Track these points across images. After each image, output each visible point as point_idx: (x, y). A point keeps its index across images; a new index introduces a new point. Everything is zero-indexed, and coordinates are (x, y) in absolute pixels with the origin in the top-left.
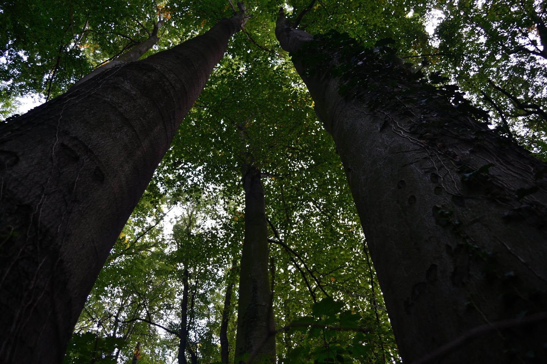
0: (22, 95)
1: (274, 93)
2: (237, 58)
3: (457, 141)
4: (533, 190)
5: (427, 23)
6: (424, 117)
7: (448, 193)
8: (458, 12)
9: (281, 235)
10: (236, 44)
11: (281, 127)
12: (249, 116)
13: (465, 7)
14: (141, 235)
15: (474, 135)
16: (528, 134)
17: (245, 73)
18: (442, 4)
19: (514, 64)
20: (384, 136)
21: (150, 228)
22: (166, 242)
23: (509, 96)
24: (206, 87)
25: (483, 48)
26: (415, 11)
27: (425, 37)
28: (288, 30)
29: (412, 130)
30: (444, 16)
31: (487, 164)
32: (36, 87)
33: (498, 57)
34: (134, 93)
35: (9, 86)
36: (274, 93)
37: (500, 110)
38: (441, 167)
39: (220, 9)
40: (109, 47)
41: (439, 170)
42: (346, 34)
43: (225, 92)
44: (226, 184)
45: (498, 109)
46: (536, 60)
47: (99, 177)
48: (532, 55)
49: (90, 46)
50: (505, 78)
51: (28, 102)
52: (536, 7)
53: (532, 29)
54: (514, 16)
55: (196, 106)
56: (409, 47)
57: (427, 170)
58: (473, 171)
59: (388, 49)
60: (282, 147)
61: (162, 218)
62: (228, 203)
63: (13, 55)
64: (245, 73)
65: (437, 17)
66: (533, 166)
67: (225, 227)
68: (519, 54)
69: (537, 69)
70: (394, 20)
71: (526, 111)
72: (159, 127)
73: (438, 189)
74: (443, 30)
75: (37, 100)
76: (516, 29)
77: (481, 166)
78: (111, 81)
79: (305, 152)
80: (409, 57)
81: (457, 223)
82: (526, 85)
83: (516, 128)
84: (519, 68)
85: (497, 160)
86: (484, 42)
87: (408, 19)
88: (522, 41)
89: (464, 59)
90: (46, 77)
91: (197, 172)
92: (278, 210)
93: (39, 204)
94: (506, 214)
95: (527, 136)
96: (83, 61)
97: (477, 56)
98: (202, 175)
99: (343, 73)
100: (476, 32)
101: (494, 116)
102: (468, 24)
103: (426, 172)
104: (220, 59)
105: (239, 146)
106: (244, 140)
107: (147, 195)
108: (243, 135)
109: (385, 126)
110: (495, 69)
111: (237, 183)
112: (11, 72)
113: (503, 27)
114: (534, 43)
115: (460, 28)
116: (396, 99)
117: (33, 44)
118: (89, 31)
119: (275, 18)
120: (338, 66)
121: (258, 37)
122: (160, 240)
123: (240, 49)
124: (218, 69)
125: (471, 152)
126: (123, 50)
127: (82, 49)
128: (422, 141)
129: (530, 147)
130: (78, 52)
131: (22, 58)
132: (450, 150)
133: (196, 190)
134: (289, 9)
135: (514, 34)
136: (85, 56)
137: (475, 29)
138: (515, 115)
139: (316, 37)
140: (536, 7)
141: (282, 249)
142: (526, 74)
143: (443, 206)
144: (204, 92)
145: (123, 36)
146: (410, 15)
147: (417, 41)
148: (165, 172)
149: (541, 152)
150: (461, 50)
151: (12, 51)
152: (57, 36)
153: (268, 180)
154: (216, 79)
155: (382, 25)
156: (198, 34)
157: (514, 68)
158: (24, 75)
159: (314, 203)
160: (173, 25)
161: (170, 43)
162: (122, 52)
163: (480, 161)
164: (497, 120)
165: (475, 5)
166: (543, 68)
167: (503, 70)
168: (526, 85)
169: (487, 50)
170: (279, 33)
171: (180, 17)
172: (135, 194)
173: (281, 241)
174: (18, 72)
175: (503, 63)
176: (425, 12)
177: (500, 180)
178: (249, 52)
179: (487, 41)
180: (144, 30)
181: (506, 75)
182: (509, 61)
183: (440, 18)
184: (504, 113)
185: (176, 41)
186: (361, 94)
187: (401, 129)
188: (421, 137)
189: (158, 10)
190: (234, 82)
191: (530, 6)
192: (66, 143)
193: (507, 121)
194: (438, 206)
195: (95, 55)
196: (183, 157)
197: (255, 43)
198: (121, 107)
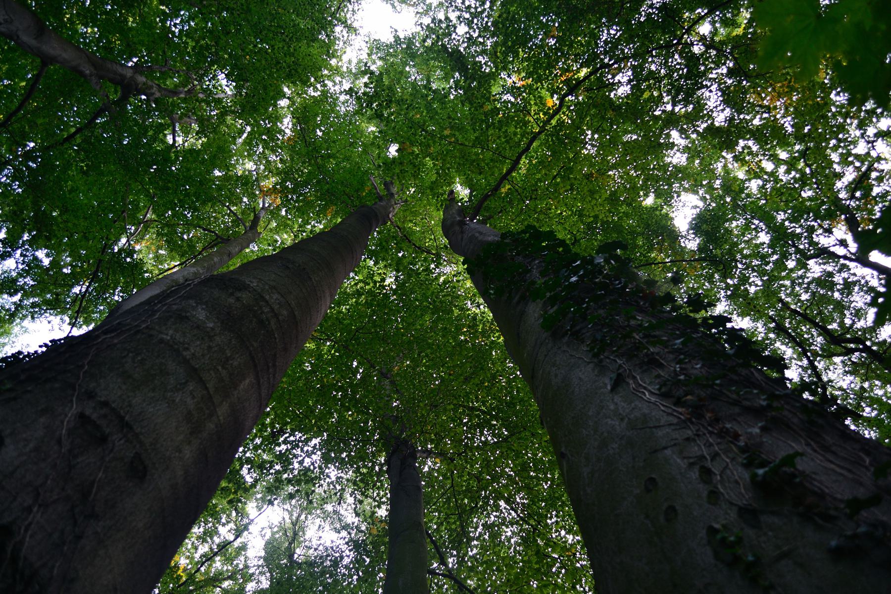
0: (33, 318)
1: (439, 319)
2: (382, 264)
3: (737, 410)
4: (875, 500)
5: (675, 214)
6: (681, 369)
7: (731, 504)
8: (722, 197)
9: (451, 560)
10: (381, 243)
11: (450, 375)
12: (398, 356)
13: (731, 190)
14: (208, 558)
15: (764, 400)
16: (853, 386)
17: (394, 287)
18: (696, 186)
19: (816, 276)
20: (617, 399)
21: (224, 546)
22: (251, 571)
23: (816, 325)
24: (331, 308)
25: (766, 250)
26: (658, 196)
27: (673, 236)
28: (462, 223)
29: (663, 390)
30: (701, 204)
31: (791, 452)
32: (55, 306)
33: (791, 264)
34: (211, 325)
35: (15, 303)
36: (439, 319)
37: (802, 346)
38: (714, 457)
39: (357, 191)
40: (181, 246)
41: (712, 460)
42: (551, 235)
43: (360, 317)
44: (357, 471)
45: (800, 345)
46: (850, 270)
47: (138, 471)
48: (842, 261)
49: (152, 244)
50: (804, 297)
51: (37, 333)
52: (839, 191)
53: (838, 223)
54: (808, 204)
55: (314, 339)
56: (651, 249)
57: (691, 460)
58: (770, 463)
59: (617, 258)
60: (452, 406)
61: (246, 528)
62: (361, 502)
63: (27, 256)
64: (394, 287)
65: (691, 205)
66: (868, 454)
67: (356, 545)
68: (822, 259)
69: (854, 283)
70: (624, 208)
71: (845, 348)
72: (247, 381)
73: (714, 496)
74: (700, 224)
75: (56, 327)
76: (813, 223)
77: (782, 454)
78: (175, 307)
79: (491, 415)
80: (651, 264)
81: (750, 558)
82: (840, 307)
83: (831, 375)
84: (826, 281)
85: (808, 444)
86: (767, 242)
87: (646, 208)
88: (824, 241)
89: (737, 267)
90: (76, 290)
91: (310, 449)
92: (446, 514)
93: (27, 523)
94: (833, 543)
95: (852, 390)
96: (138, 266)
97: (757, 263)
98: (319, 453)
99: (548, 295)
100: (753, 226)
101: (795, 356)
102: (740, 214)
103: (691, 465)
104: (354, 265)
105: (381, 405)
106: (389, 396)
107: (223, 489)
108: (388, 387)
109: (618, 382)
110: (787, 283)
111: (377, 468)
112: (21, 282)
113: (794, 219)
114: (843, 243)
115: (727, 221)
116: (634, 337)
117: (61, 240)
118: (152, 221)
119: (442, 205)
120: (540, 281)
121: (414, 232)
122: (241, 566)
123: (386, 250)
124: (352, 281)
125: (763, 429)
126: (203, 250)
127: (137, 247)
128: (680, 410)
129: (859, 406)
130: (131, 252)
131: (41, 261)
132: (728, 426)
133: (307, 478)
134: (463, 192)
135: (811, 230)
136: (140, 259)
137: (750, 222)
138: (828, 355)
139: (504, 236)
140: (839, 191)
141: (452, 587)
142: (838, 290)
143: (724, 526)
144: (326, 318)
145: (204, 230)
146: (650, 201)
147: (663, 240)
148: (256, 448)
149: (878, 415)
150: (731, 253)
151: (27, 250)
152: (101, 229)
153: (430, 463)
154: (346, 296)
155: (607, 217)
156: (322, 227)
157: (818, 282)
158: (41, 287)
159: (507, 502)
160: (283, 213)
161: (276, 241)
162: (200, 253)
163: (780, 447)
164: (800, 363)
165: (747, 188)
166: (863, 282)
167: (800, 284)
168: (840, 307)
169: (773, 253)
170: (447, 228)
171: (296, 202)
172: (204, 487)
173: (450, 571)
174: (32, 283)
175: (800, 273)
176: (672, 197)
177: (815, 480)
178: (400, 255)
179: (771, 240)
180: (237, 221)
181: (806, 292)
182: (807, 270)
183: (696, 207)
184: (810, 351)
185: (287, 239)
186: (578, 328)
187: (645, 388)
188: (678, 402)
189: (261, 191)
190: (377, 300)
191: (829, 189)
192: (88, 412)
193: (816, 363)
194: (717, 526)
195: (158, 258)
196: (288, 423)
197: (410, 242)
198: (187, 349)
